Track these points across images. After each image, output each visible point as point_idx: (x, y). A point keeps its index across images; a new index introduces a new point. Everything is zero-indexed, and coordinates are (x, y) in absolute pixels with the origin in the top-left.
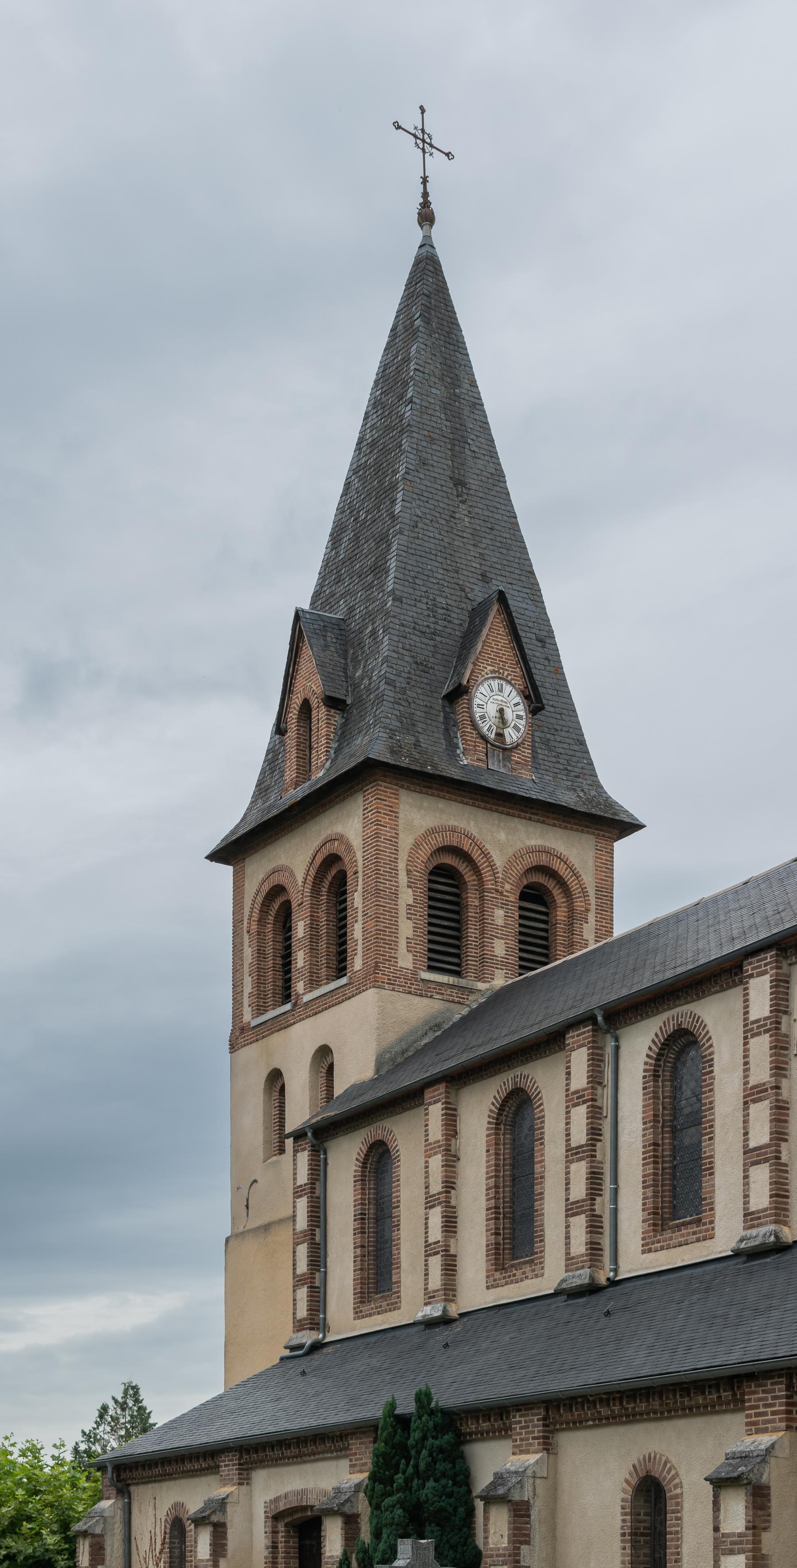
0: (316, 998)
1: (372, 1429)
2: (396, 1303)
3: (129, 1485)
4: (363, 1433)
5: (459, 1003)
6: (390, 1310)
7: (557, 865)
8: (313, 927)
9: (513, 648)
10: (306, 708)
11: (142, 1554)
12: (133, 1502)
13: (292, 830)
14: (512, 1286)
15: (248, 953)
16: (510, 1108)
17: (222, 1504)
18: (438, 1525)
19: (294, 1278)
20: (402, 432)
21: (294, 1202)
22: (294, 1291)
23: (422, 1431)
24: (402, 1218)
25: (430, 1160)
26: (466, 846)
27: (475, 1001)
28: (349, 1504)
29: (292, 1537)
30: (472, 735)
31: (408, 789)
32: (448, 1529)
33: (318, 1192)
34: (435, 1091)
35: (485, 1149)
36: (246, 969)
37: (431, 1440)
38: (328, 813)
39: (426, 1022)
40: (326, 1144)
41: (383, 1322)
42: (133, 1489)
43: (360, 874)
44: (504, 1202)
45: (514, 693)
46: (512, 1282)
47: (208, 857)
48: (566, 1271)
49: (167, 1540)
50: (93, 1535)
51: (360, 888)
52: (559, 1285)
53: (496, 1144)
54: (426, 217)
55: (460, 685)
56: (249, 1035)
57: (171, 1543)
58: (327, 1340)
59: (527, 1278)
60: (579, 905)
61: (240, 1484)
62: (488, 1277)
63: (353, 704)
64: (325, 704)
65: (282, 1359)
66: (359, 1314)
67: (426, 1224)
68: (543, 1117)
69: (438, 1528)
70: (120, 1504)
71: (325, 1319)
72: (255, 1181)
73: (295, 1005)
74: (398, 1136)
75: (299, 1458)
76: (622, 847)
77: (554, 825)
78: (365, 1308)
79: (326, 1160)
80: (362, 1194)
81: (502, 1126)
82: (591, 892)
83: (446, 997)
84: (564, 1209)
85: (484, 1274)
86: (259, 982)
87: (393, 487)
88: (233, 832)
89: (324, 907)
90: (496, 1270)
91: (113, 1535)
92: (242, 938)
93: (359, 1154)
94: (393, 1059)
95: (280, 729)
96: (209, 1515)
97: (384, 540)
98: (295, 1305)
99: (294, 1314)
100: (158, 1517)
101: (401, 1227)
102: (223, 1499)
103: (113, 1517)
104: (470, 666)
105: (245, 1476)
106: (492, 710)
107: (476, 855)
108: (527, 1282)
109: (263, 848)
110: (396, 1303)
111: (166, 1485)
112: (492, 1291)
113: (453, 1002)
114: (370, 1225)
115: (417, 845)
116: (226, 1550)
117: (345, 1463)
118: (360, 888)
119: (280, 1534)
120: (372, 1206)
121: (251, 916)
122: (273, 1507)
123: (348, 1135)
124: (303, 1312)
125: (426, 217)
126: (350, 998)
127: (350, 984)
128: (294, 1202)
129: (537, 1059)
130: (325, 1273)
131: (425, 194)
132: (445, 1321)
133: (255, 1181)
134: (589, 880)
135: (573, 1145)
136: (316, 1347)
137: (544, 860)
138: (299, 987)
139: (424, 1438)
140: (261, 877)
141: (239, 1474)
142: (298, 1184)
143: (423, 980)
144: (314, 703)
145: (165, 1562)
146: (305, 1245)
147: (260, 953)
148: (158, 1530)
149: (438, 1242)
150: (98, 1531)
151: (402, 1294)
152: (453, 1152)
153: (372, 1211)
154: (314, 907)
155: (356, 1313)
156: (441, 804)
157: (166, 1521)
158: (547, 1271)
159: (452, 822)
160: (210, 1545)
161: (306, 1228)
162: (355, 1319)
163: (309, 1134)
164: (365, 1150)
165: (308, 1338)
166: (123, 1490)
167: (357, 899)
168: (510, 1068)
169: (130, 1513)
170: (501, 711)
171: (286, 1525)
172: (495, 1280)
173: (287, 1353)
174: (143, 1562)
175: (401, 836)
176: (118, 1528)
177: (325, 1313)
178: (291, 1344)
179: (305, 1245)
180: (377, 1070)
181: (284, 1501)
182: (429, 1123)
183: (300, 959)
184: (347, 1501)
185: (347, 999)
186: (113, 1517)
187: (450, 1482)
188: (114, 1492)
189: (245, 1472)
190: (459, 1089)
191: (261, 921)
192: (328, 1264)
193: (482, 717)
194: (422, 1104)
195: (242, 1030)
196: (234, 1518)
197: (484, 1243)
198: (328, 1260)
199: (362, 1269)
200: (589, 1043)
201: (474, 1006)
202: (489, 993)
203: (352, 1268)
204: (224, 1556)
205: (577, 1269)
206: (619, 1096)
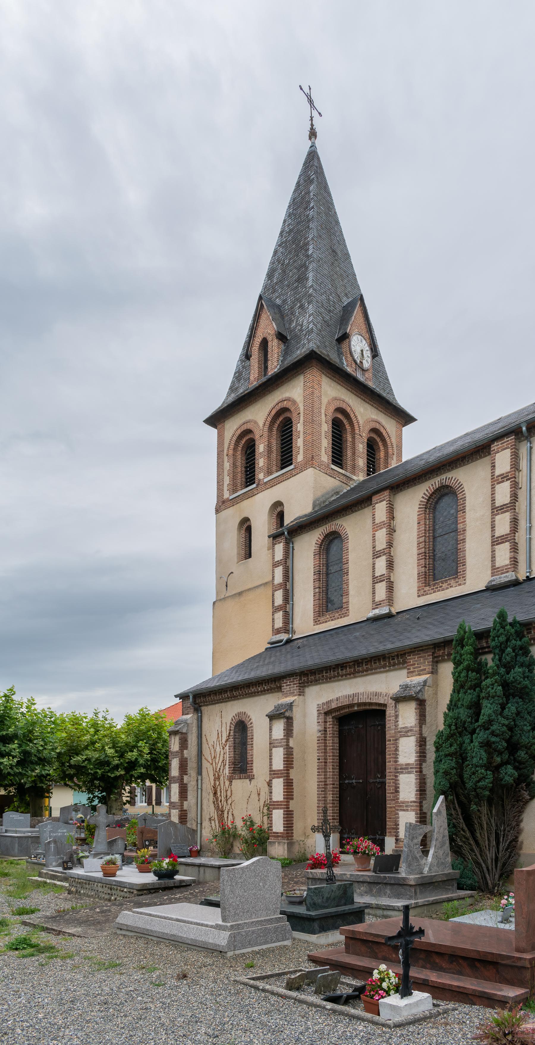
0: (275, 478)
1: (432, 646)
2: (346, 613)
3: (200, 706)
4: (422, 650)
5: (346, 484)
6: (341, 617)
7: (382, 430)
8: (269, 446)
9: (365, 324)
10: (264, 343)
11: (211, 743)
12: (203, 715)
13: (256, 401)
14: (439, 593)
15: (227, 465)
16: (433, 500)
17: (290, 706)
18: (520, 698)
19: (273, 608)
20: (309, 221)
21: (273, 570)
22: (273, 615)
23: (506, 636)
24: (350, 569)
25: (376, 533)
26: (348, 410)
27: (353, 485)
28: (421, 693)
29: (335, 725)
30: (350, 359)
31: (326, 375)
32: (527, 701)
33: (289, 563)
34: (380, 496)
35: (416, 522)
36: (226, 473)
37: (513, 642)
38: (279, 389)
39: (333, 490)
40: (293, 539)
41: (336, 624)
42: (203, 708)
43: (302, 415)
44: (429, 550)
45: (366, 345)
46: (439, 591)
47: (204, 421)
48: (492, 576)
49: (232, 734)
50: (182, 733)
51: (301, 421)
52: (488, 583)
53: (425, 519)
54: (313, 134)
55: (346, 333)
56: (227, 504)
57: (235, 735)
58: (293, 638)
59: (451, 587)
60: (390, 450)
61: (300, 695)
62: (419, 590)
63: (291, 339)
64: (277, 338)
65: (266, 649)
66: (316, 622)
67: (373, 567)
68: (465, 497)
69: (521, 700)
70: (196, 717)
71: (292, 628)
72: (232, 573)
73: (258, 485)
74: (346, 527)
75: (354, 674)
76: (407, 430)
77: (381, 411)
78: (322, 619)
79: (293, 547)
80: (320, 561)
81: (428, 510)
82: (395, 446)
83: (341, 480)
84: (490, 541)
85: (416, 589)
86: (234, 478)
87: (307, 244)
88: (220, 408)
89: (275, 437)
90: (425, 586)
91: (192, 733)
92: (223, 459)
93: (317, 541)
94: (320, 504)
95: (247, 356)
96: (285, 712)
97: (304, 267)
98: (273, 622)
99: (273, 626)
100: (224, 722)
101: (349, 573)
102: (291, 703)
103: (192, 724)
104: (350, 326)
105: (302, 690)
106: (358, 351)
107: (352, 415)
108: (451, 589)
109: (237, 413)
110: (346, 613)
111: (230, 704)
112: (422, 598)
113: (343, 483)
114: (323, 577)
115: (329, 403)
116: (292, 733)
117: (405, 672)
118: (301, 421)
119: (328, 723)
120: (324, 567)
121: (229, 447)
122: (325, 707)
123: (309, 533)
124: (279, 623)
125: (313, 134)
126: (295, 475)
127: (295, 468)
128: (273, 570)
129: (461, 466)
130: (293, 604)
131: (312, 125)
132: (389, 616)
133: (232, 573)
134: (394, 440)
135: (497, 505)
136: (289, 641)
137: (378, 426)
138: (260, 476)
139: (508, 640)
140: (235, 428)
141: (299, 689)
142: (276, 560)
143: (332, 469)
144: (270, 339)
145: (229, 746)
146: (282, 590)
147: (234, 465)
148: (224, 729)
149: (384, 575)
150: (184, 731)
151: (350, 608)
152: (392, 527)
153: (324, 570)
154: (270, 437)
155: (316, 622)
156: (339, 387)
157: (231, 723)
158: (468, 581)
159: (343, 397)
160: (284, 730)
161: (281, 581)
162: (314, 625)
163: (286, 533)
164: (322, 538)
165: (284, 637)
166: (197, 709)
167: (299, 427)
168: (437, 475)
169: (201, 721)
170: (362, 351)
171: (333, 718)
172: (424, 592)
173: (269, 646)
174: (211, 748)
175: (323, 397)
176: (194, 730)
177: (292, 624)
178: (272, 641)
179: (282, 590)
180: (314, 508)
181: (335, 702)
182: (376, 513)
183: (261, 462)
184: (420, 691)
185: (293, 476)
186: (192, 724)
187: (527, 670)
188: (192, 710)
189: (302, 688)
190: (395, 494)
191: (235, 449)
192: (294, 600)
193: (355, 351)
194: (371, 504)
195: (224, 502)
196: (297, 714)
197: (416, 572)
198: (294, 598)
199: (319, 599)
200: (511, 446)
201: (352, 486)
202: (358, 482)
203: (312, 599)
204: (292, 737)
205: (502, 574)
206: (532, 475)
